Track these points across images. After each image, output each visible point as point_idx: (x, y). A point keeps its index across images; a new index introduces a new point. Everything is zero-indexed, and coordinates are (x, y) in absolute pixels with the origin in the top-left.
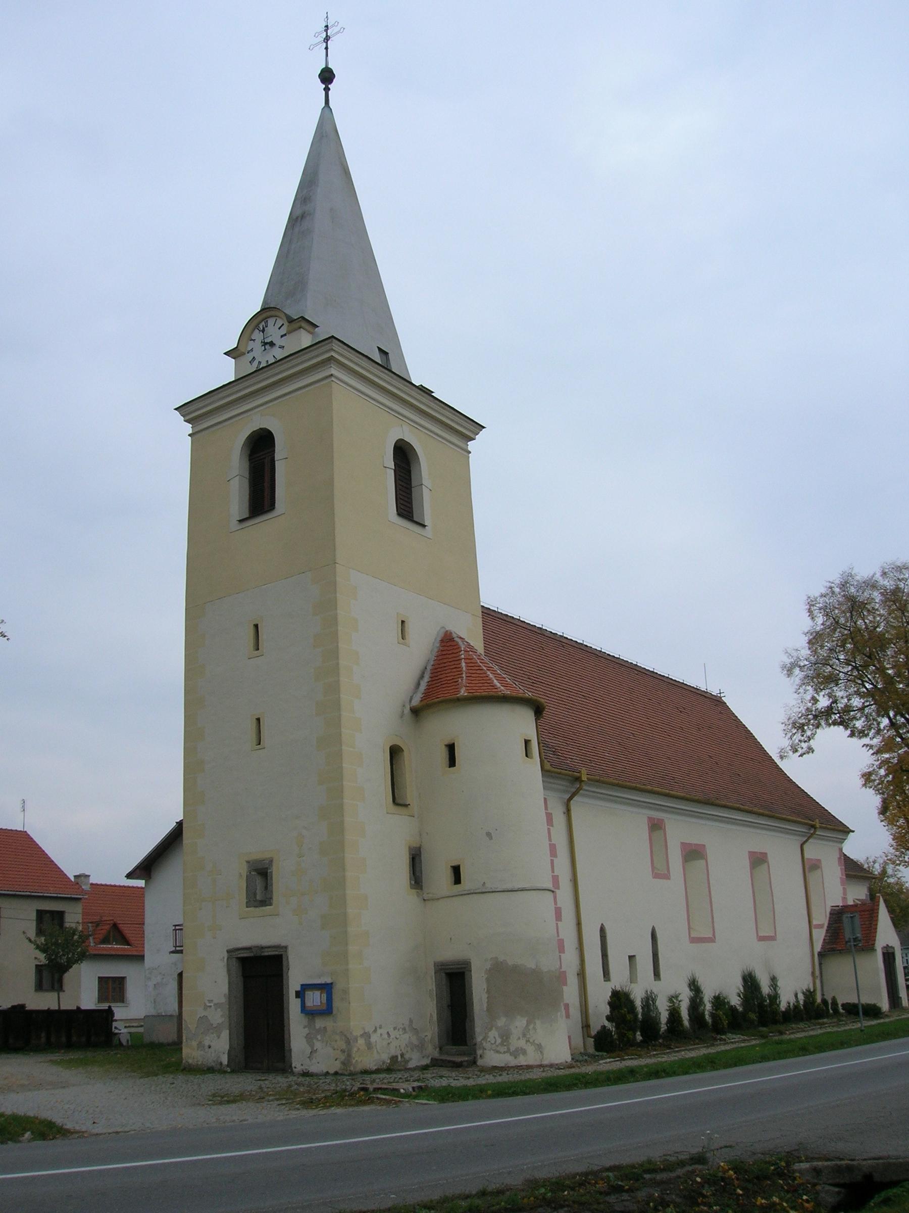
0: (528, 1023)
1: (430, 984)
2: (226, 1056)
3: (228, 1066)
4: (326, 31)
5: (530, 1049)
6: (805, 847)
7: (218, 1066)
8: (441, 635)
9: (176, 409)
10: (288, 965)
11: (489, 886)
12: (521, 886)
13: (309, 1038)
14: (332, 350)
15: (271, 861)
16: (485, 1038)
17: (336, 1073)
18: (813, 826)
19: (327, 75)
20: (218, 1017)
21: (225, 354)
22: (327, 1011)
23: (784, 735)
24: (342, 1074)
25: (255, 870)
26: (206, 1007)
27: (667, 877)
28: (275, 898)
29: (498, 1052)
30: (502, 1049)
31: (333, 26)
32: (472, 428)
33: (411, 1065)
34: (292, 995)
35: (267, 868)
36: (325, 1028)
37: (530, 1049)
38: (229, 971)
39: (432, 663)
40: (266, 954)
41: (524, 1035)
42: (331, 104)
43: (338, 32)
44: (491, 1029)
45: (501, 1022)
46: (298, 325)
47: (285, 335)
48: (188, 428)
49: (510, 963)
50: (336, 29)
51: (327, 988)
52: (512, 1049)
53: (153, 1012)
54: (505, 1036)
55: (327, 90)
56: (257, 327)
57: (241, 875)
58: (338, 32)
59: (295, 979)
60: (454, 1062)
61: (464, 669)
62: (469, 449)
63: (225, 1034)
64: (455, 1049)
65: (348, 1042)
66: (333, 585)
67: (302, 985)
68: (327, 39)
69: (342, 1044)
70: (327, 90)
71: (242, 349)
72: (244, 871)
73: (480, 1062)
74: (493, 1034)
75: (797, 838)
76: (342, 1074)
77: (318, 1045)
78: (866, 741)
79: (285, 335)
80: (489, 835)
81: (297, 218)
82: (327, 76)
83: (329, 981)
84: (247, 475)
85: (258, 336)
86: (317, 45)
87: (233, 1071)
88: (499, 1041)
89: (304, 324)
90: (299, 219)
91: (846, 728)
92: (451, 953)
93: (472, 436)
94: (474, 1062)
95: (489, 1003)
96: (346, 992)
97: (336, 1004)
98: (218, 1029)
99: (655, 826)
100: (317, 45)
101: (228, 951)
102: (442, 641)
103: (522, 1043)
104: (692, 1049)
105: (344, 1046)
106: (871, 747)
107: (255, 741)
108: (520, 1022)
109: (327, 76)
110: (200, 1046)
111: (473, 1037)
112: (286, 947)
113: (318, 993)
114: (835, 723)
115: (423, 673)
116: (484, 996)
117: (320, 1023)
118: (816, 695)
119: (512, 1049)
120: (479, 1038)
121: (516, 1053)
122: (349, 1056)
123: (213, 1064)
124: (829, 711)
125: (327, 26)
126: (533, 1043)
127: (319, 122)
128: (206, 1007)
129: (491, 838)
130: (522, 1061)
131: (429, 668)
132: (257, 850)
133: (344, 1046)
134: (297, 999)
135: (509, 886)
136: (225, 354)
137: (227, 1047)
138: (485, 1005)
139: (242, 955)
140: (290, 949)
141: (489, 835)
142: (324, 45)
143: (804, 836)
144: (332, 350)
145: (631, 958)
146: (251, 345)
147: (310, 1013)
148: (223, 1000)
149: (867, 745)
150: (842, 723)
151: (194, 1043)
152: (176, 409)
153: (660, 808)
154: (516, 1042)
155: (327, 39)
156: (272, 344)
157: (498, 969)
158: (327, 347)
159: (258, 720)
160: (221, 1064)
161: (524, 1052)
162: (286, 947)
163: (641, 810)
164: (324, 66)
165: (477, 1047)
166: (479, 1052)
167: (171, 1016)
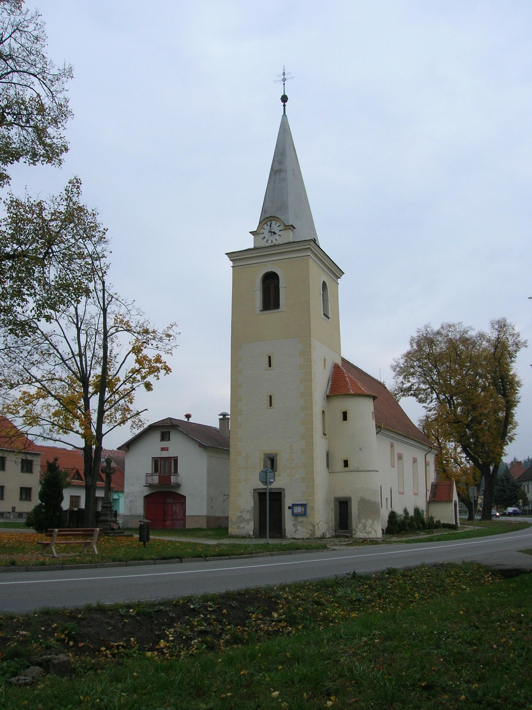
0: (373, 522)
1: (332, 506)
2: (252, 532)
3: (253, 535)
4: (284, 75)
5: (373, 532)
6: (427, 456)
7: (248, 536)
8: (334, 365)
9: (226, 254)
10: (285, 496)
11: (360, 469)
12: (371, 469)
13: (295, 525)
14: (311, 245)
15: (276, 454)
16: (357, 527)
17: (307, 538)
18: (431, 448)
19: (285, 99)
20: (247, 516)
21: (250, 232)
22: (304, 514)
23: (174, 351)
24: (310, 539)
25: (268, 457)
26: (241, 512)
27: (394, 467)
28: (278, 469)
29: (362, 532)
30: (363, 531)
31: (288, 74)
32: (340, 273)
33: (327, 536)
34: (286, 508)
35: (274, 457)
36: (303, 521)
37: (373, 532)
38: (254, 498)
39: (331, 376)
40: (273, 491)
41: (371, 526)
42: (286, 114)
43: (291, 78)
44: (359, 524)
45: (363, 521)
46: (290, 227)
47: (282, 230)
48: (231, 263)
49: (367, 499)
50: (290, 76)
51: (304, 506)
52: (367, 531)
53: (129, 514)
54: (365, 527)
55: (284, 106)
56: (266, 223)
57: (261, 459)
58: (291, 78)
59: (288, 501)
60: (346, 536)
61: (348, 381)
62: (338, 282)
63: (252, 523)
64: (342, 531)
65: (314, 527)
66: (310, 345)
67: (292, 504)
68: (284, 80)
69: (311, 528)
70: (284, 106)
71: (258, 232)
72: (263, 457)
73: (354, 536)
74: (360, 526)
75: (423, 452)
76: (310, 539)
77: (299, 528)
78: (425, 405)
79: (282, 230)
80: (360, 449)
81: (277, 171)
82: (284, 99)
83: (305, 503)
84: (262, 290)
85: (267, 228)
86: (279, 81)
87: (255, 538)
88: (362, 528)
89: (292, 228)
90: (278, 172)
91: (417, 397)
92: (341, 494)
93: (339, 276)
94: (352, 536)
95: (359, 514)
96: (313, 507)
97: (308, 511)
98: (248, 521)
99: (392, 446)
100: (279, 81)
101: (253, 490)
102: (334, 367)
103: (370, 529)
104: (410, 536)
105: (311, 528)
106: (427, 408)
107: (269, 405)
108: (370, 521)
109: (284, 99)
110: (238, 527)
111: (351, 526)
112: (284, 489)
113: (300, 508)
114: (411, 395)
115: (329, 381)
116: (357, 511)
117: (300, 519)
118: (404, 381)
119: (367, 531)
120: (354, 527)
121: (368, 533)
122: (314, 532)
123: (245, 535)
124: (410, 389)
125: (284, 73)
126: (374, 530)
127: (281, 122)
128: (241, 512)
129: (361, 450)
130: (370, 536)
131: (330, 378)
132: (270, 449)
133: (311, 528)
134: (289, 510)
135: (367, 469)
136: (250, 232)
137: (253, 528)
138: (357, 514)
139: (260, 491)
140: (286, 490)
141: (360, 449)
142: (283, 83)
143: (426, 451)
144: (311, 245)
145: (387, 498)
146: (263, 231)
147: (295, 515)
148: (251, 509)
149: (425, 407)
150: (414, 395)
151: (235, 526)
152: (226, 254)
153: (394, 438)
154: (368, 529)
155: (284, 80)
156: (274, 233)
157: (363, 502)
158: (309, 243)
159: (271, 397)
160: (249, 535)
161: (371, 533)
162: (284, 489)
163: (389, 439)
164: (283, 94)
165: (353, 530)
166: (354, 532)
167: (139, 516)
